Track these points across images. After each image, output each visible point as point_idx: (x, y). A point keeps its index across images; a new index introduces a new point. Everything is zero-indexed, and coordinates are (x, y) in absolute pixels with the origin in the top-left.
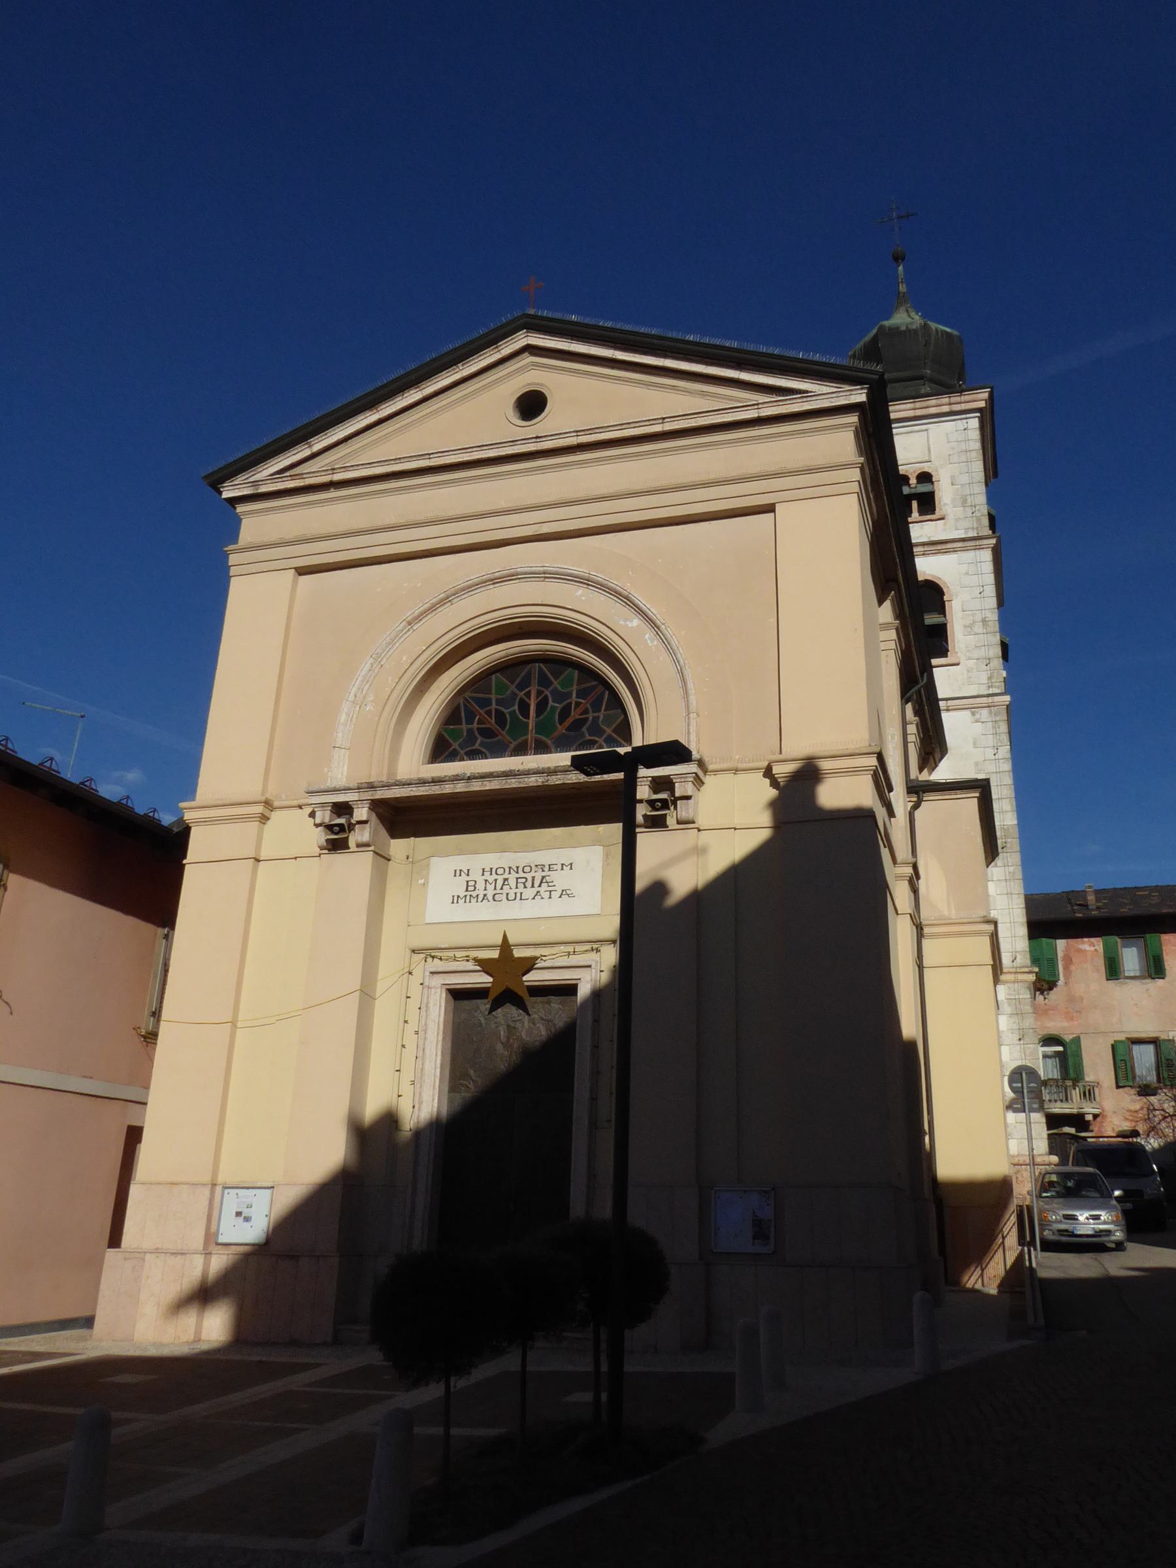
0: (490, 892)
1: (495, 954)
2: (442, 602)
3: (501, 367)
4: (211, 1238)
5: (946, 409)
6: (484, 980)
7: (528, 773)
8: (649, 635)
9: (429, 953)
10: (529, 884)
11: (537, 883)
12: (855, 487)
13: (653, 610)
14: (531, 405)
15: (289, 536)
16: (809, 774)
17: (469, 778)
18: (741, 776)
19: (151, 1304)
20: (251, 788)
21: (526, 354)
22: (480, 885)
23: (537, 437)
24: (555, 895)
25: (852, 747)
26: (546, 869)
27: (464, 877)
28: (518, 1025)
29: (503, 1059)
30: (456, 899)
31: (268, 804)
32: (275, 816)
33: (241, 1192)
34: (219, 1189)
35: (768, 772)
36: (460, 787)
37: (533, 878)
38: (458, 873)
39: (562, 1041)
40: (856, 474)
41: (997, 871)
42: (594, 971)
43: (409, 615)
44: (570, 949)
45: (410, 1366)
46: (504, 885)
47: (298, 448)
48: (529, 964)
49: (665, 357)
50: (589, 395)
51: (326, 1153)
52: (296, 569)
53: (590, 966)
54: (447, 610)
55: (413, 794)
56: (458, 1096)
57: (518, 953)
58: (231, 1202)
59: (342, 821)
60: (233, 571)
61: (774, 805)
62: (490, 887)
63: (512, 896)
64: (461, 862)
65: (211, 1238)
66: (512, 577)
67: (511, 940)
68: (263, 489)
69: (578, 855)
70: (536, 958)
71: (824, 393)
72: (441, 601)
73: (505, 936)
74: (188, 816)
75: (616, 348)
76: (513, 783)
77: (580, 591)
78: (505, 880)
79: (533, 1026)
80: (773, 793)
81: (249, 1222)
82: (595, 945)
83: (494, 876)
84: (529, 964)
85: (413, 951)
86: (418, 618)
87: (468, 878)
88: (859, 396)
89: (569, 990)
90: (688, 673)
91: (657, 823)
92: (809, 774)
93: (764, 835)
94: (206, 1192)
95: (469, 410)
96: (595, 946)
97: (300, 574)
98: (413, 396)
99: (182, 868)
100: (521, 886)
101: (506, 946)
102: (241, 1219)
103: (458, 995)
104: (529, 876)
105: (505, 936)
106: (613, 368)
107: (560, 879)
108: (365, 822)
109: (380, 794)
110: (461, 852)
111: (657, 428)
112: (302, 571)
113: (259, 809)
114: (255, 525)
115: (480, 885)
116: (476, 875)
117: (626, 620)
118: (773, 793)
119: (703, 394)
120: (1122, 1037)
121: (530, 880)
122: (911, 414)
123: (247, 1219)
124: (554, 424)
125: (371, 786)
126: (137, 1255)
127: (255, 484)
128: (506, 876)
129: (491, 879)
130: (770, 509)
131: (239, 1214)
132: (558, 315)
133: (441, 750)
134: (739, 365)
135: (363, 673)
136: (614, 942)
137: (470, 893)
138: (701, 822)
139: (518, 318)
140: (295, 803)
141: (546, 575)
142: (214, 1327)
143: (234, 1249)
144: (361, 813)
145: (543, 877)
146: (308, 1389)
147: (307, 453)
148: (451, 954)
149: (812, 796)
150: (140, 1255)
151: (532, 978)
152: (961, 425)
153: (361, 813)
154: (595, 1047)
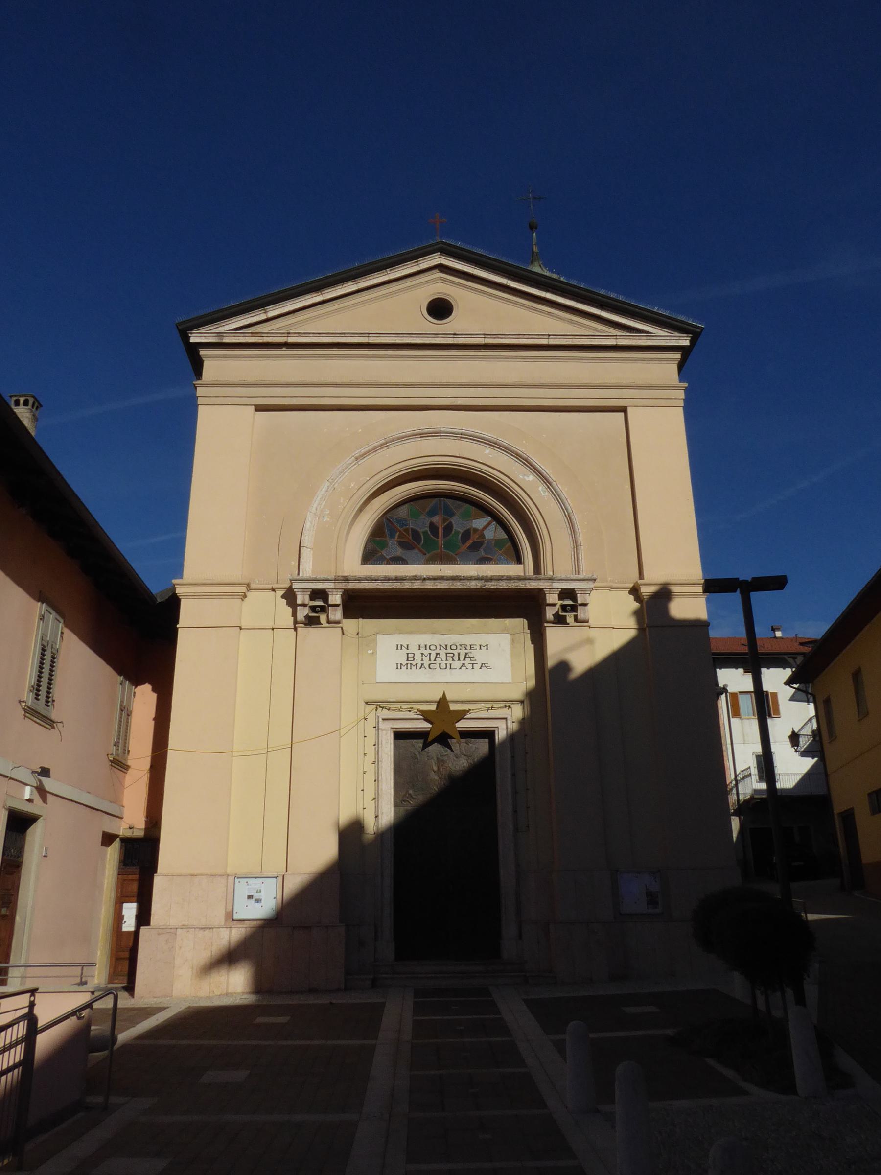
0: (426, 662)
1: (433, 707)
2: (382, 446)
3: (417, 277)
4: (230, 916)
6: (425, 726)
7: (470, 579)
8: (541, 487)
9: (378, 704)
10: (456, 658)
11: (462, 658)
13: (548, 471)
14: (440, 309)
15: (251, 379)
16: (664, 594)
17: (425, 579)
18: (614, 593)
19: (189, 968)
20: (235, 571)
21: (437, 270)
22: (418, 657)
23: (455, 334)
24: (477, 667)
26: (469, 647)
27: (405, 651)
28: (445, 758)
29: (435, 781)
30: (399, 666)
32: (250, 595)
33: (250, 881)
35: (635, 591)
36: (417, 585)
37: (459, 654)
38: (399, 647)
39: (484, 770)
40: (681, 394)
42: (506, 722)
43: (357, 453)
44: (489, 705)
46: (436, 657)
47: (256, 312)
48: (462, 715)
49: (547, 291)
50: (483, 310)
51: (324, 851)
52: (255, 406)
54: (384, 452)
55: (379, 587)
56: (402, 808)
57: (453, 707)
58: (243, 889)
59: (321, 603)
60: (200, 401)
61: (637, 614)
62: (426, 659)
63: (443, 666)
64: (403, 639)
65: (230, 916)
67: (449, 698)
68: (227, 340)
69: (492, 639)
70: (469, 711)
71: (661, 336)
72: (382, 445)
73: (444, 694)
74: (179, 590)
75: (509, 278)
76: (458, 585)
77: (488, 451)
78: (437, 654)
79: (461, 759)
80: (636, 605)
81: (260, 901)
82: (508, 703)
83: (428, 651)
84: (462, 715)
85: (367, 703)
86: (363, 456)
87: (408, 651)
88: (685, 342)
89: (489, 735)
90: (576, 518)
91: (560, 620)
92: (664, 594)
93: (631, 634)
95: (391, 303)
96: (508, 704)
97: (256, 410)
98: (350, 287)
99: (176, 630)
101: (443, 702)
102: (252, 901)
103: (399, 736)
104: (456, 652)
105: (444, 694)
106: (504, 292)
107: (480, 656)
108: (337, 605)
109: (351, 586)
110: (400, 632)
111: (544, 342)
112: (259, 408)
113: (243, 589)
114: (214, 366)
115: (418, 657)
116: (414, 649)
117: (525, 475)
118: (636, 605)
119: (571, 322)
121: (456, 655)
123: (258, 901)
124: (457, 325)
125: (346, 579)
126: (169, 931)
127: (220, 335)
128: (438, 651)
129: (426, 652)
130: (624, 410)
131: (250, 897)
132: (468, 247)
133: (370, 556)
134: (601, 306)
135: (322, 493)
136: (522, 702)
137: (410, 662)
138: (592, 623)
139: (438, 243)
140: (270, 587)
141: (462, 436)
142: (235, 986)
143: (247, 924)
145: (466, 654)
146: (147, 1042)
147: (263, 317)
148: (398, 706)
149: (666, 610)
150: (171, 931)
151: (462, 725)
154: (514, 775)
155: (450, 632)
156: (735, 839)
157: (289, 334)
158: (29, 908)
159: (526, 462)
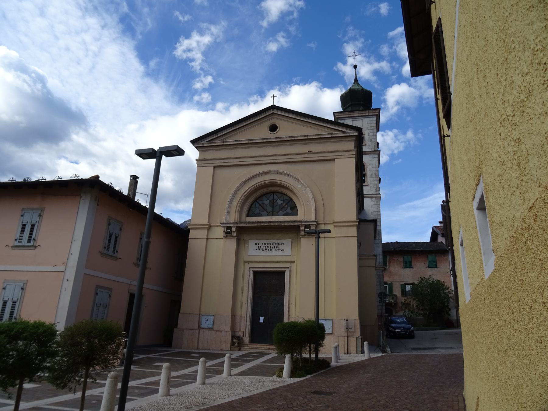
0: (264, 249)
5: (367, 114)
12: (354, 156)
14: (273, 128)
22: (262, 247)
25: (352, 220)
30: (256, 250)
40: (354, 153)
45: (375, 346)
64: (257, 241)
66: (269, 173)
68: (205, 145)
69: (285, 241)
94: (198, 316)
107: (281, 247)
109: (238, 225)
113: (207, 226)
115: (262, 247)
116: (261, 245)
120: (403, 283)
122: (358, 115)
124: (281, 133)
127: (203, 144)
130: (334, 160)
137: (259, 249)
144: (234, 229)
147: (216, 136)
152: (371, 119)
153: (234, 229)
155: (273, 239)
156: (445, 243)
157: (224, 142)
158: (411, 204)
159: (292, 176)
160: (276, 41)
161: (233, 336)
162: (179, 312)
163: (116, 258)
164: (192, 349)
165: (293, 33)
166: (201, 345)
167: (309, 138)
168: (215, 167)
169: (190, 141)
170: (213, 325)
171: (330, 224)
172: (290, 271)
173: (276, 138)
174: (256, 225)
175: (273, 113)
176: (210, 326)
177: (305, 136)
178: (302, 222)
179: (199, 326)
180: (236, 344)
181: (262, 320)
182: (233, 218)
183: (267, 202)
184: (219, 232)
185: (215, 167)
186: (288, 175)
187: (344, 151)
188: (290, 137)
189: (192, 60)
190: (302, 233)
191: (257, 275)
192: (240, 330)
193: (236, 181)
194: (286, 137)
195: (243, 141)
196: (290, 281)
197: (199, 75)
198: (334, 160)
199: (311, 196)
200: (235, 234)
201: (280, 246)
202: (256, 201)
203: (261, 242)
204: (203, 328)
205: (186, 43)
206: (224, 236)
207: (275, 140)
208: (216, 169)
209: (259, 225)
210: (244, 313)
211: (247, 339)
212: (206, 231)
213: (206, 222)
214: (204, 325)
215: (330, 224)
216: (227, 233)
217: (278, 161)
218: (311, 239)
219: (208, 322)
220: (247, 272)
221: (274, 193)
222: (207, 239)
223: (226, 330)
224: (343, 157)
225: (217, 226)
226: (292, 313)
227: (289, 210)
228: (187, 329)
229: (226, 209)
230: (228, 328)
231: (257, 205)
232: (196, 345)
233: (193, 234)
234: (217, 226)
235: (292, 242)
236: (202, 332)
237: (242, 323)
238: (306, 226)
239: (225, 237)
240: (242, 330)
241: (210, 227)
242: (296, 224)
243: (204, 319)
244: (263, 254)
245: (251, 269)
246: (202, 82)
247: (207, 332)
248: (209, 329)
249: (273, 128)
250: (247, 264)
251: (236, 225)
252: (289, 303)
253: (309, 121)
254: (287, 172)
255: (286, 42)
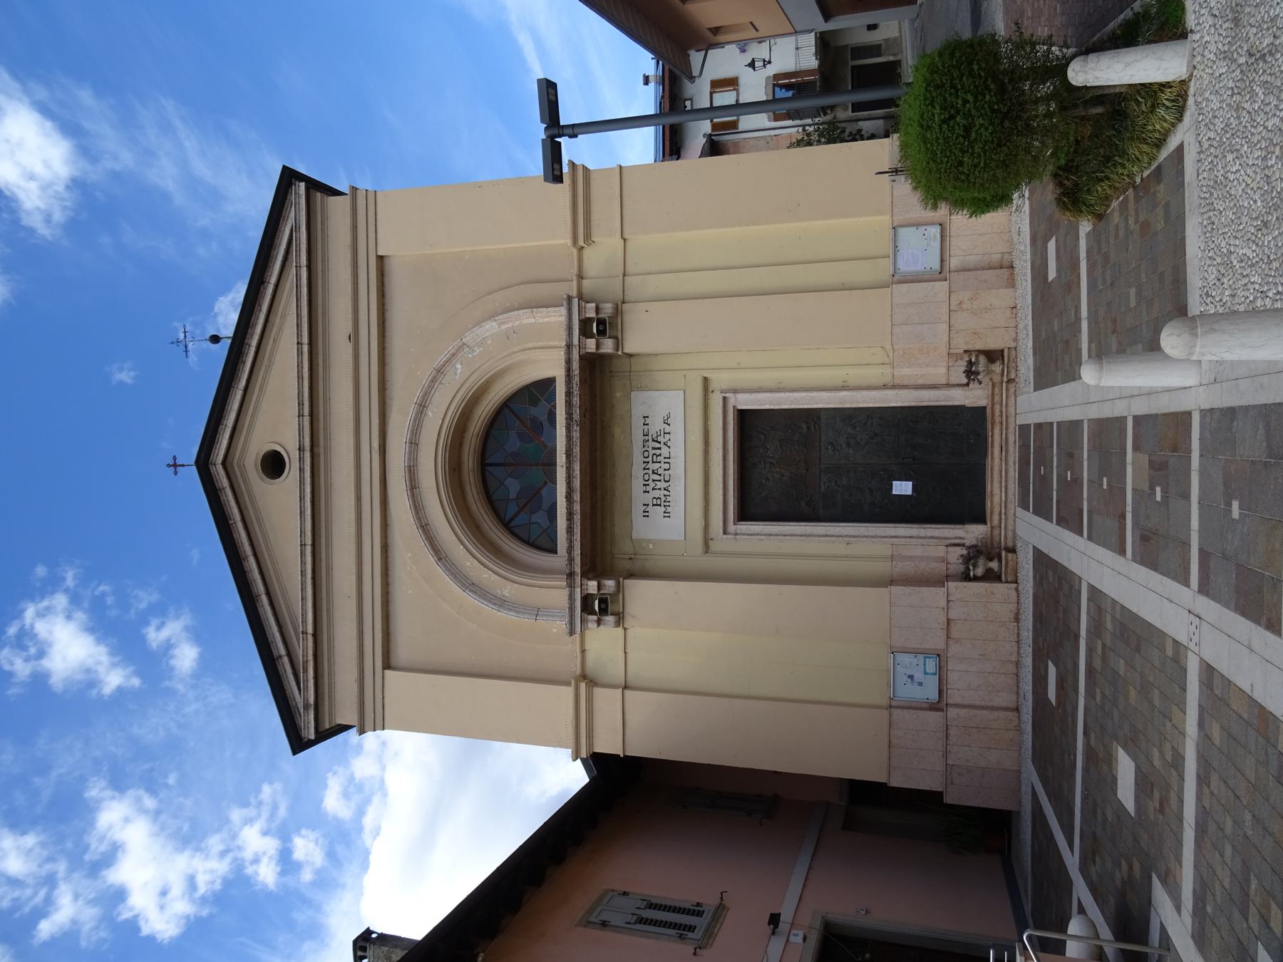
0: (664, 485)
7: (569, 437)
10: (658, 452)
11: (657, 445)
14: (274, 465)
22: (657, 494)
24: (668, 429)
31: (584, 676)
34: (894, 703)
41: (776, 945)
52: (384, 668)
53: (724, 398)
62: (659, 485)
63: (667, 466)
64: (637, 510)
68: (312, 700)
69: (637, 411)
94: (896, 712)
100: (659, 459)
109: (578, 570)
113: (583, 685)
115: (657, 494)
116: (648, 498)
127: (306, 707)
141: (414, 443)
147: (286, 659)
153: (592, 586)
160: (168, 646)
161: (966, 577)
162: (882, 786)
163: (721, 909)
164: (1019, 729)
165: (155, 597)
166: (1005, 699)
167: (305, 340)
168: (387, 665)
169: (295, 752)
170: (926, 653)
171: (580, 260)
172: (735, 391)
173: (301, 449)
174: (577, 507)
175: (224, 463)
176: (931, 665)
177: (300, 353)
178: (569, 347)
179: (934, 707)
180: (994, 565)
181: (903, 488)
182: (556, 595)
183: (513, 486)
184: (603, 640)
185: (387, 665)
186: (422, 407)
187: (354, 227)
188: (301, 404)
189: (191, 882)
190: (608, 346)
191: (749, 507)
192: (943, 560)
193: (442, 587)
194: (301, 415)
195: (303, 563)
196: (771, 391)
197: (239, 866)
198: (381, 259)
199: (491, 327)
200: (610, 584)
201: (653, 432)
202: (507, 526)
203: (639, 496)
204: (940, 692)
205: (141, 901)
206: (618, 624)
207: (307, 455)
208: (394, 662)
209: (577, 497)
210: (882, 548)
211: (973, 533)
212: (598, 691)
213: (568, 692)
214: (930, 692)
215: (580, 260)
216: (604, 611)
217: (376, 444)
218: (627, 318)
219: (919, 676)
220: (744, 545)
221: (483, 464)
222: (626, 687)
223: (943, 603)
224: (371, 229)
225: (583, 651)
226: (876, 374)
227: (539, 412)
228: (946, 754)
229: (526, 621)
230: (935, 596)
231: (522, 519)
232: (1002, 714)
233: (608, 744)
234: (583, 651)
235: (641, 389)
236: (954, 697)
237: (918, 552)
238: (585, 331)
239: (620, 619)
240: (941, 551)
241: (588, 679)
242: (576, 365)
243: (908, 692)
244: (679, 483)
245: (731, 528)
246: (256, 861)
247: (954, 677)
248: (941, 671)
249: (274, 465)
250: (714, 546)
251: (578, 579)
252: (844, 388)
253: (254, 343)
254: (412, 410)
255: (177, 617)
